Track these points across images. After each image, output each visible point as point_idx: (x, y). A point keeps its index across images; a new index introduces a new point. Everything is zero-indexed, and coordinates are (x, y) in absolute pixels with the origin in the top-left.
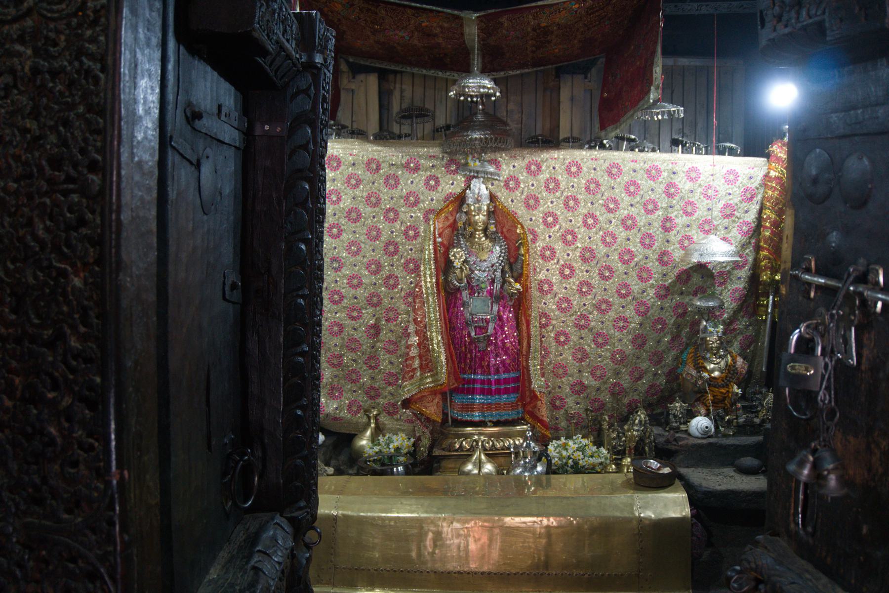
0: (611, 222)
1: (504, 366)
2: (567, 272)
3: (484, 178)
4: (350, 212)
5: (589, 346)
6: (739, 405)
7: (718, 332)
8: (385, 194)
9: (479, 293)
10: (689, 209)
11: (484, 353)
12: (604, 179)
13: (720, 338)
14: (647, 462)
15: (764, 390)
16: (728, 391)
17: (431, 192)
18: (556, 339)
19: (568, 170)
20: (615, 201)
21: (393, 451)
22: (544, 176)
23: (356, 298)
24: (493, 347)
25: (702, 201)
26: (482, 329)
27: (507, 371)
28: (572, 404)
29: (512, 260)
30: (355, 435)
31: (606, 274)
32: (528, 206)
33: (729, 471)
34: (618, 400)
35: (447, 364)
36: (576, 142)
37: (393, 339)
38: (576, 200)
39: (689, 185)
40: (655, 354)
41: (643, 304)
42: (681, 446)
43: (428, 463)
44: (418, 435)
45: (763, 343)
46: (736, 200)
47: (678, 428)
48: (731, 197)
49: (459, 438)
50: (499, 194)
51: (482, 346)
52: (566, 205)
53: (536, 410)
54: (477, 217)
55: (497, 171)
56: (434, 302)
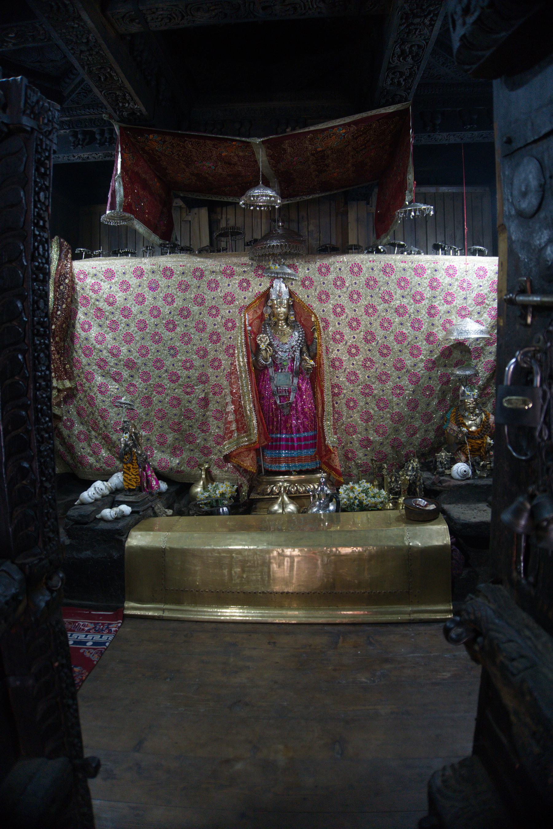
0: (387, 311)
1: (304, 427)
3: (282, 278)
4: (182, 310)
5: (373, 409)
7: (473, 395)
8: (209, 295)
9: (282, 369)
10: (449, 298)
11: (288, 418)
12: (381, 278)
13: (476, 400)
14: (416, 501)
16: (483, 442)
17: (244, 292)
19: (352, 271)
21: (219, 495)
22: (331, 277)
24: (294, 412)
25: (460, 292)
26: (284, 398)
27: (306, 430)
29: (309, 343)
30: (193, 484)
32: (320, 300)
34: (397, 451)
35: (258, 426)
36: (357, 249)
37: (219, 408)
38: (358, 294)
39: (448, 280)
40: (425, 415)
41: (415, 375)
42: (444, 487)
43: (246, 505)
47: (443, 472)
48: (481, 288)
49: (270, 485)
50: (298, 292)
51: (286, 411)
54: (279, 309)
55: (294, 273)
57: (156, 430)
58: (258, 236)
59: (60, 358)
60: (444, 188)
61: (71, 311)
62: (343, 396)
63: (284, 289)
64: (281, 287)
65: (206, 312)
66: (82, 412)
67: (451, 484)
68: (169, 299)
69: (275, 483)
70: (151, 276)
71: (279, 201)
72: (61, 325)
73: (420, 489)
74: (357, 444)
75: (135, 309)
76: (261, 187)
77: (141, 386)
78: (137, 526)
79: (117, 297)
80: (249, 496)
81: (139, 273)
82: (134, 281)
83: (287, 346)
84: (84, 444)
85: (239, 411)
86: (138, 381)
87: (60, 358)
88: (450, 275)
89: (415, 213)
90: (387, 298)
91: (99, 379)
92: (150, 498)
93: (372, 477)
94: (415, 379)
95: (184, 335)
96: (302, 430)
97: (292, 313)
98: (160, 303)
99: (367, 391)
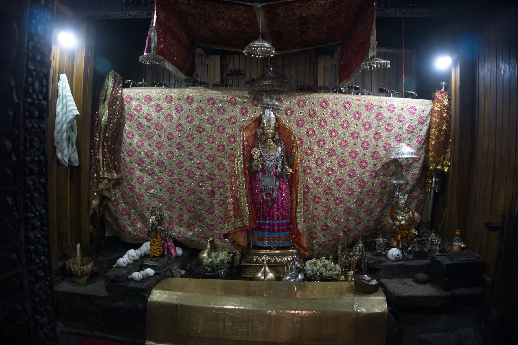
0: (345, 134)
2: (320, 162)
3: (272, 108)
4: (199, 127)
6: (415, 240)
7: (405, 198)
9: (268, 174)
11: (271, 209)
12: (341, 110)
13: (406, 202)
15: (429, 231)
16: (410, 232)
17: (243, 117)
20: (348, 123)
21: (219, 262)
23: (201, 175)
24: (276, 205)
27: (284, 219)
28: (321, 237)
29: (288, 155)
31: (342, 164)
32: (298, 125)
33: (410, 281)
34: (347, 235)
35: (249, 214)
36: (325, 89)
37: (222, 198)
40: (368, 209)
41: (363, 181)
42: (383, 266)
43: (237, 271)
45: (429, 204)
46: (415, 123)
47: (381, 253)
51: (270, 204)
52: (320, 124)
55: (280, 105)
56: (242, 179)
57: (177, 212)
58: (254, 77)
59: (111, 157)
60: (385, 49)
61: (120, 124)
62: (310, 194)
63: (272, 116)
64: (270, 114)
65: (216, 130)
66: (125, 195)
67: (388, 264)
68: (190, 119)
69: (261, 255)
70: (178, 102)
71: (273, 52)
72: (113, 134)
73: (365, 266)
74: (319, 228)
75: (165, 125)
76: (260, 40)
77: (167, 179)
78: (158, 285)
79: (153, 116)
80: (240, 262)
81: (169, 99)
82: (165, 105)
83: (273, 157)
84: (126, 218)
85: (237, 203)
86: (165, 177)
87: (111, 157)
88: (391, 111)
89: (377, 65)
90: (346, 125)
91: (138, 173)
92: (170, 262)
93: (328, 252)
94: (362, 184)
95: (200, 145)
96: (281, 218)
97: (277, 133)
98: (183, 121)
99: (328, 191)
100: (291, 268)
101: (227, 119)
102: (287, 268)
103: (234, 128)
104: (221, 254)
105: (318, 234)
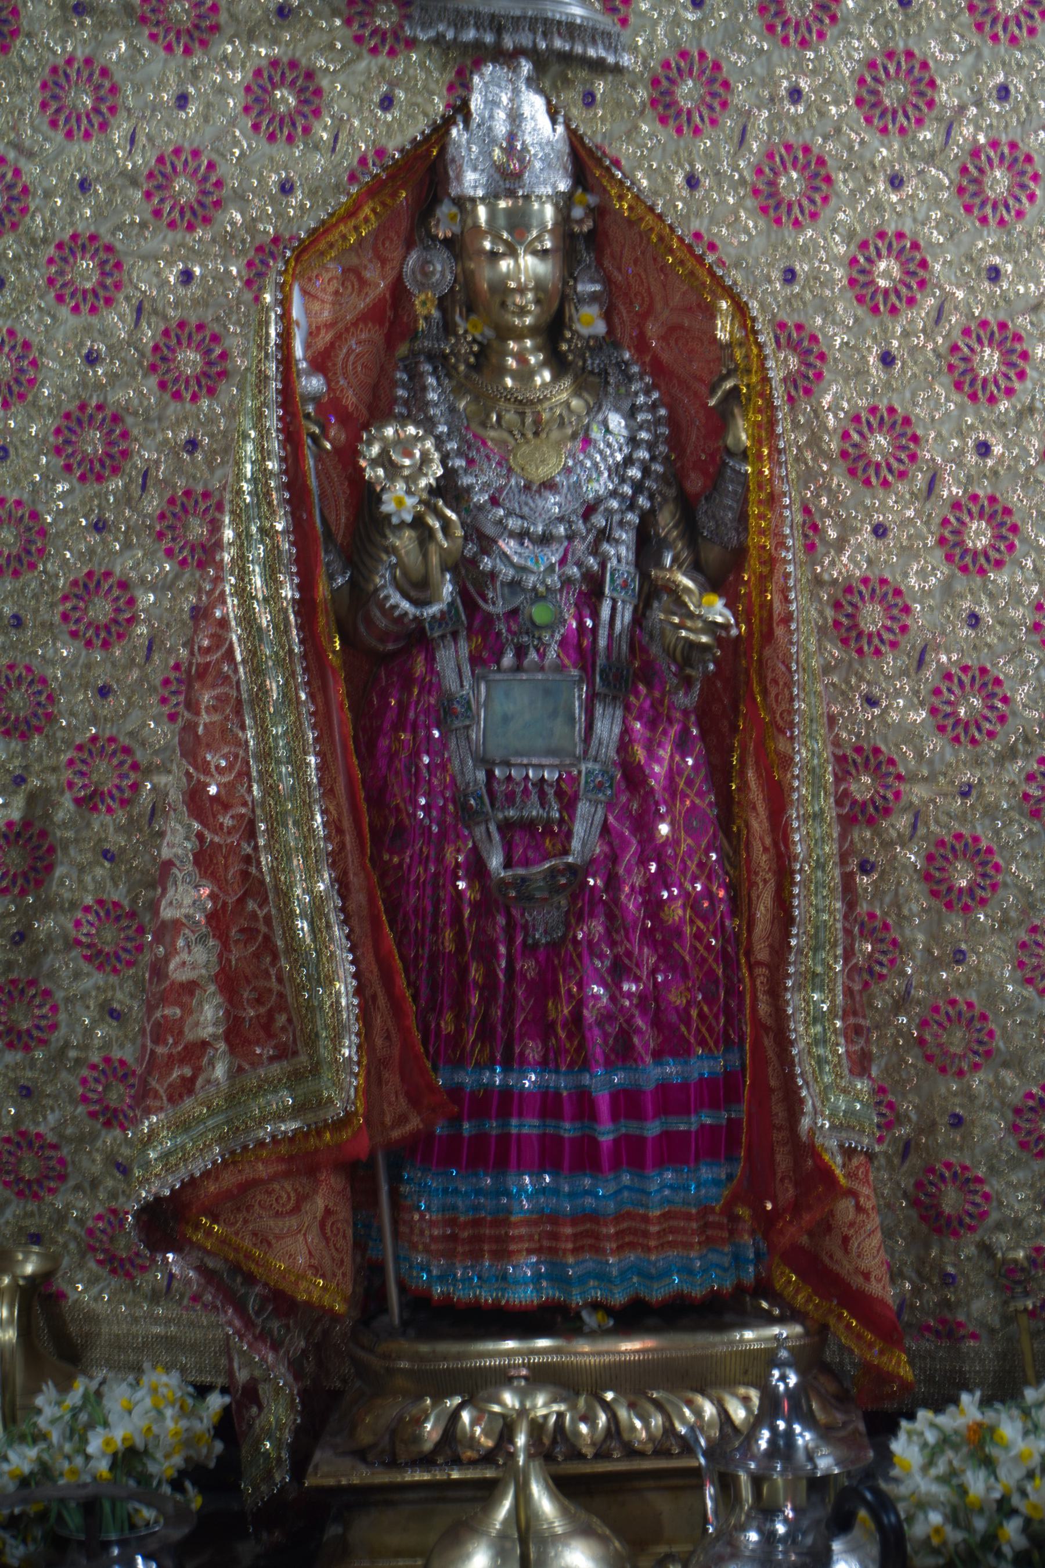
1: (657, 1023)
2: (979, 535)
9: (521, 652)
11: (557, 961)
17: (280, 151)
18: (934, 879)
21: (102, 1467)
24: (596, 927)
26: (527, 837)
27: (671, 1045)
29: (695, 483)
32: (771, 205)
35: (365, 1015)
37: (118, 894)
44: (242, 1376)
49: (438, 1398)
50: (625, 151)
51: (543, 922)
53: (832, 1244)
54: (505, 265)
56: (288, 698)
63: (540, 128)
64: (523, 116)
69: (478, 1386)
74: (993, 1128)
83: (553, 504)
85: (247, 917)
96: (645, 1038)
100: (757, 1481)
101: (133, 180)
102: (727, 1485)
103: (202, 256)
104: (118, 1396)
105: (993, 1186)
